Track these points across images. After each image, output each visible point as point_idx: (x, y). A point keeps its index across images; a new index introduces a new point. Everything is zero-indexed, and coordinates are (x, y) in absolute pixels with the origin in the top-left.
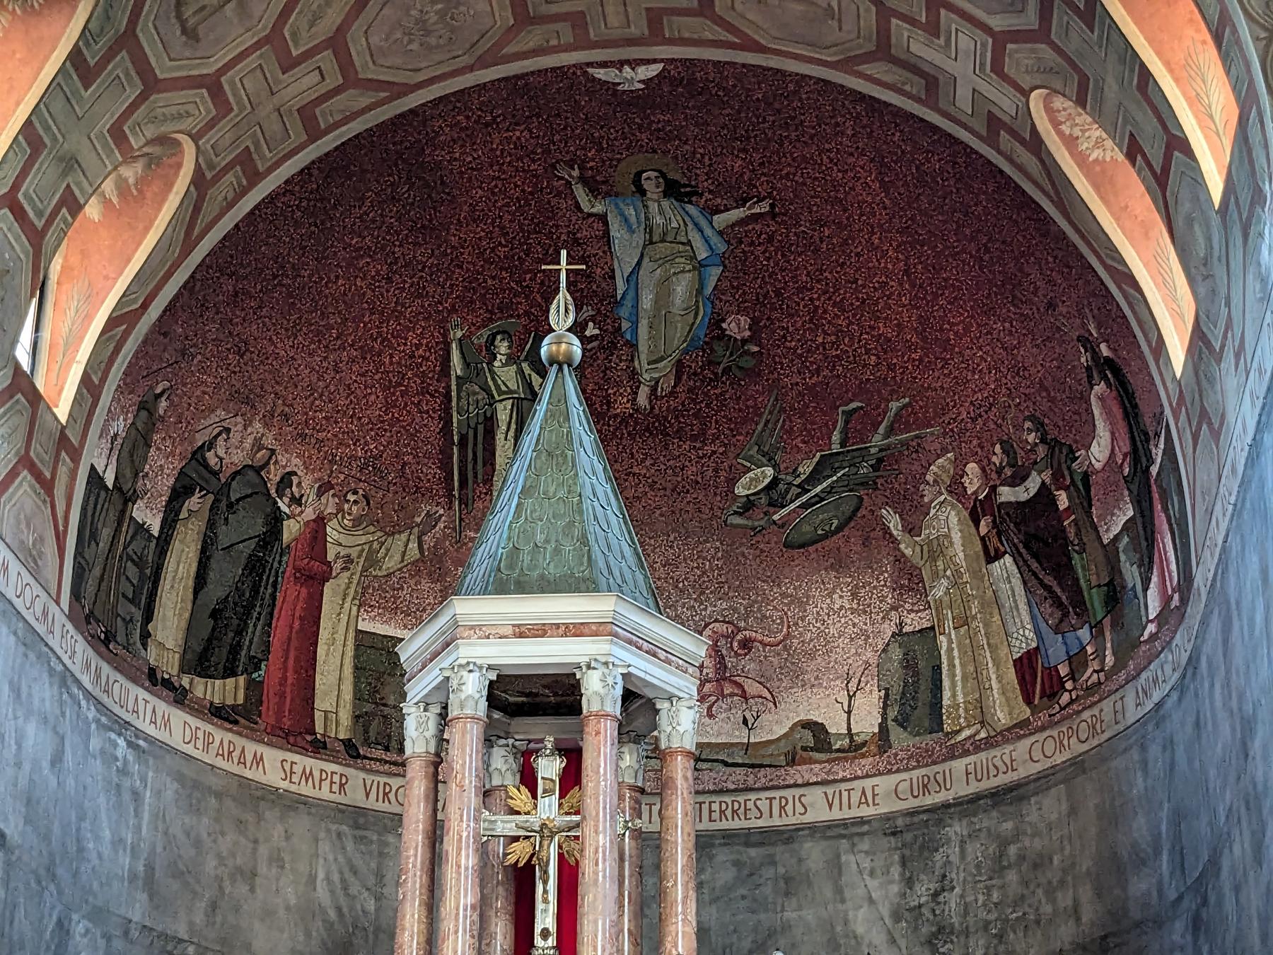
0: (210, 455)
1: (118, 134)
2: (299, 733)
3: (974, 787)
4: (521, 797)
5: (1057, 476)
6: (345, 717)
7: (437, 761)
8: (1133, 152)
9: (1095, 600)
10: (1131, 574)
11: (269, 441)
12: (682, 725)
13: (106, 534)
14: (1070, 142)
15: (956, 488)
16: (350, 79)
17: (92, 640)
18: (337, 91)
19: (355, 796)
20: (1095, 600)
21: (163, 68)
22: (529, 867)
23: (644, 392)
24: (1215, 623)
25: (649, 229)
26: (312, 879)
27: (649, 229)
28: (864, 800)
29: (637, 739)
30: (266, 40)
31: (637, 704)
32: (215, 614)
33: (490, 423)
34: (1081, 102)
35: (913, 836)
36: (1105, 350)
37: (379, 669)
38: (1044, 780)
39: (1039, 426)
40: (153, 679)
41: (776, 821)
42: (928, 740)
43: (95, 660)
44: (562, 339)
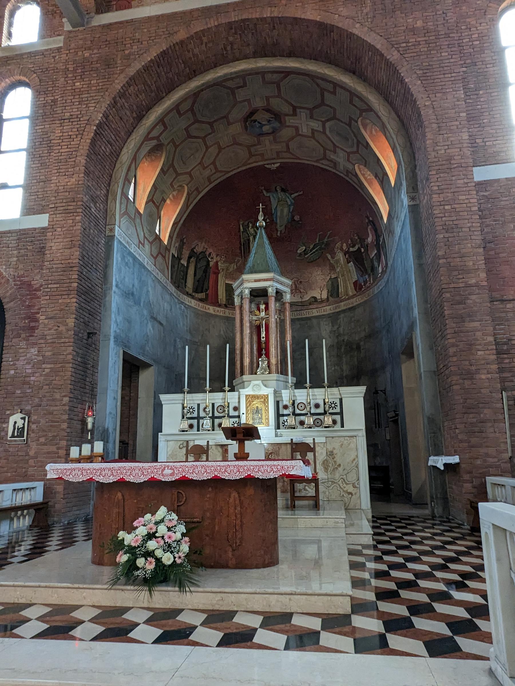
0: (195, 250)
1: (172, 186)
2: (216, 303)
3: (345, 308)
4: (257, 312)
5: (361, 245)
6: (224, 300)
7: (241, 307)
8: (376, 176)
9: (369, 271)
10: (376, 264)
11: (206, 247)
12: (288, 297)
13: (176, 266)
14: (363, 175)
15: (341, 249)
16: (217, 170)
17: (176, 287)
18: (215, 173)
19: (227, 314)
20: (369, 271)
21: (179, 171)
22: (260, 326)
23: (279, 232)
24: (392, 274)
25: (279, 199)
26: (220, 331)
27: (279, 199)
28: (324, 311)
29: (279, 300)
30: (200, 163)
31: (279, 294)
32: (198, 281)
33: (249, 240)
34: (365, 166)
35: (334, 318)
36: (371, 219)
37: (230, 291)
38: (358, 306)
39: (358, 235)
40: (187, 294)
41: (307, 316)
42: (336, 299)
43: (176, 291)
44: (261, 222)
